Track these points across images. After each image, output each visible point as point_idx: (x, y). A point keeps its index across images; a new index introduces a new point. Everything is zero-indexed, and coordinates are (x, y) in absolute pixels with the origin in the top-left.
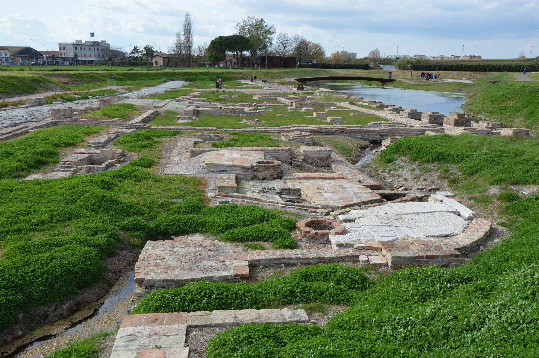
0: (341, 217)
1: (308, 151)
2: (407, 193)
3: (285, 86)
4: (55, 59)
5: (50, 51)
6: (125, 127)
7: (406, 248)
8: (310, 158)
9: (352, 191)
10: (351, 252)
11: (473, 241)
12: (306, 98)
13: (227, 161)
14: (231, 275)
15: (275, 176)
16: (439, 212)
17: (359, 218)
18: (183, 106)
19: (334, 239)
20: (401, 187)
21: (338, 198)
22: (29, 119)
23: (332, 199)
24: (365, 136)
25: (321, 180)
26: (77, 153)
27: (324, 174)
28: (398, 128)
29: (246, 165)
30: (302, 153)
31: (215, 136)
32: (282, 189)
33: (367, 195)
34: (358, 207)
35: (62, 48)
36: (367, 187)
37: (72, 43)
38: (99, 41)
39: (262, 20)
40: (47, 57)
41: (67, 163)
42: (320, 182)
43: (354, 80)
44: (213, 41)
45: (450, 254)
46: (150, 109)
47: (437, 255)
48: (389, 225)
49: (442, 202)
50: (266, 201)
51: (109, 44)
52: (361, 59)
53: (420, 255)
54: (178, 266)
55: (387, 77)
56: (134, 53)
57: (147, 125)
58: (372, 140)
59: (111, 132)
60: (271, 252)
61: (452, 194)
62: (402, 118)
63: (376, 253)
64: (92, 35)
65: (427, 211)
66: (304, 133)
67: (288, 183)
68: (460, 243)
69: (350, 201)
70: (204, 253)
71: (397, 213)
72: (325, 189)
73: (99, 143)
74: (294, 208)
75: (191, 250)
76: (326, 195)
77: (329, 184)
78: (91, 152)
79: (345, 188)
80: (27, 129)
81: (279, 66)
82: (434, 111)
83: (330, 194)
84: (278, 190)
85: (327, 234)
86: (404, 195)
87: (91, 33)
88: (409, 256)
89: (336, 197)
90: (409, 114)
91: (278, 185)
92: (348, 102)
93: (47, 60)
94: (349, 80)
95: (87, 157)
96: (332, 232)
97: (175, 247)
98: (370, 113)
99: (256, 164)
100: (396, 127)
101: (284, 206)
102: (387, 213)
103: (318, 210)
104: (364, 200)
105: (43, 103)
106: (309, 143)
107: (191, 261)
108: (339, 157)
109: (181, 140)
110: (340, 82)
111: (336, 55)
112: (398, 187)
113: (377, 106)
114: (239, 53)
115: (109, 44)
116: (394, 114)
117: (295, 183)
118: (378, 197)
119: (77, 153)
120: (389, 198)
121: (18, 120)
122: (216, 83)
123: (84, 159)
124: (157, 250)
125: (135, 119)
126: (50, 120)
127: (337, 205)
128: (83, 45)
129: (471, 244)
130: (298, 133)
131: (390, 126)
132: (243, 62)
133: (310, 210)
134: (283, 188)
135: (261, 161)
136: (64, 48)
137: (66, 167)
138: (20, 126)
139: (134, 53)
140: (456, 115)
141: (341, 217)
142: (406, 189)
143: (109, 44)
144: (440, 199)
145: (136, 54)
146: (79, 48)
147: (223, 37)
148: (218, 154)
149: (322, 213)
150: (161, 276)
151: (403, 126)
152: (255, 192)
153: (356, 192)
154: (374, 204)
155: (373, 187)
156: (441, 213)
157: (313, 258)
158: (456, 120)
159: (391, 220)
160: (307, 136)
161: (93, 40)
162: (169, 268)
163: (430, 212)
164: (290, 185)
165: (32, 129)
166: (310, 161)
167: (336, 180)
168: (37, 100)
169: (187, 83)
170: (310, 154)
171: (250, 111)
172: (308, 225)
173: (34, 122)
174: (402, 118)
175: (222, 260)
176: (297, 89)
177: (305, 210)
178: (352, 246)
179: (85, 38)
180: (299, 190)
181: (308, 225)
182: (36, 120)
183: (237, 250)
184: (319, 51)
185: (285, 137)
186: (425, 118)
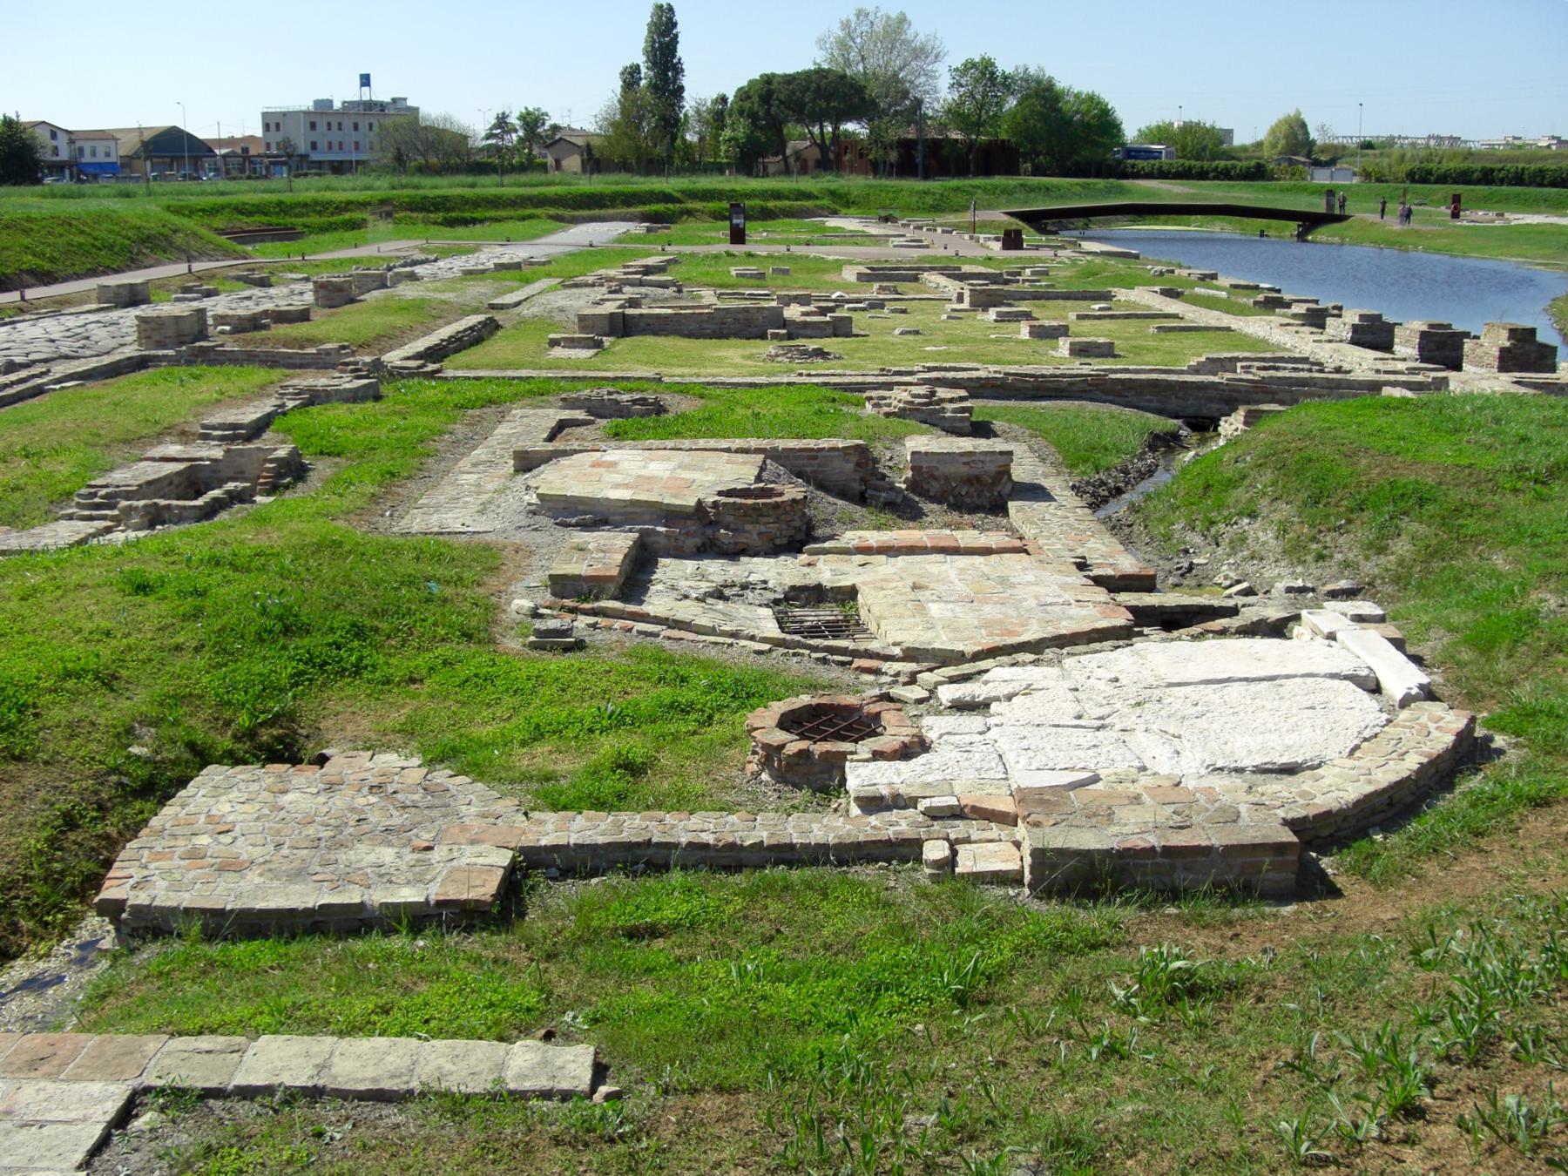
0: (947, 693)
1: (926, 454)
2: (1244, 606)
3: (967, 237)
4: (251, 162)
5: (238, 135)
6: (353, 371)
7: (1103, 815)
8: (936, 479)
9: (1036, 597)
10: (899, 825)
11: (1369, 789)
12: (1019, 274)
13: (616, 486)
14: (427, 902)
15: (778, 542)
16: (1303, 676)
17: (1009, 698)
18: (582, 302)
19: (862, 775)
20: (1238, 582)
21: (976, 623)
22: (64, 350)
23: (951, 626)
24: (1174, 403)
25: (940, 557)
26: (153, 459)
27: (958, 534)
28: (1294, 375)
29: (677, 502)
30: (909, 458)
31: (634, 402)
32: (793, 588)
33: (1084, 612)
34: (1030, 657)
35: (273, 127)
36: (1098, 581)
37: (304, 108)
38: (388, 99)
39: (902, 20)
40: (224, 156)
41: (103, 492)
42: (933, 565)
43: (1209, 217)
44: (740, 89)
45: (1257, 841)
46: (476, 311)
47: (1204, 843)
48: (1099, 723)
49: (1334, 639)
50: (712, 631)
51: (417, 109)
52: (1244, 149)
53: (1142, 844)
54: (261, 860)
55: (1319, 206)
56: (496, 136)
57: (431, 367)
58: (1196, 417)
59: (291, 390)
60: (611, 818)
61: (1379, 611)
62: (1320, 341)
63: (995, 830)
64: (365, 80)
65: (1262, 674)
66: (942, 393)
67: (820, 565)
68: (1319, 800)
69: (1010, 633)
70: (374, 817)
71: (1151, 681)
72: (941, 588)
73: (234, 426)
74: (803, 655)
75: (339, 802)
76: (935, 609)
77: (963, 571)
78: (198, 455)
79: (1012, 586)
80: (40, 381)
81: (962, 171)
82: (1436, 321)
83: (950, 606)
84: (779, 589)
85: (842, 756)
86: (1233, 612)
87: (362, 76)
88: (1099, 846)
89: (966, 616)
90: (1355, 328)
91: (782, 572)
92: (1157, 289)
93: (226, 164)
94: (1193, 217)
95: (179, 473)
96: (864, 748)
97: (285, 792)
98: (1218, 324)
99: (717, 498)
100: (1286, 374)
101: (766, 647)
102: (1117, 680)
103: (885, 666)
104: (1065, 628)
105: (140, 298)
106: (958, 425)
107: (316, 844)
108: (1046, 476)
109: (515, 416)
110: (1166, 223)
111: (1162, 133)
112: (1228, 583)
113: (1256, 303)
114: (829, 129)
115: (417, 109)
116: (1295, 329)
117: (846, 567)
118: (1122, 619)
119: (153, 459)
120: (1172, 621)
121: (27, 354)
122: (728, 223)
123: (169, 480)
124: (223, 798)
125: (406, 347)
126: (131, 351)
127: (959, 647)
128: (337, 113)
129: (1357, 803)
130: (922, 390)
131: (1265, 369)
132: (832, 157)
133: (858, 662)
134: (798, 582)
135: (739, 486)
136: (278, 126)
137: (98, 507)
138: (23, 374)
139: (496, 136)
140: (1505, 334)
141: (947, 693)
142: (1249, 592)
143: (417, 109)
144: (1326, 631)
145: (503, 139)
146: (322, 126)
147: (774, 75)
148: (596, 465)
149: (897, 674)
150: (187, 895)
151: (1310, 370)
152: (686, 597)
153: (1049, 600)
154: (1097, 646)
155: (1115, 584)
156: (1311, 680)
157: (752, 845)
158: (1503, 350)
159: (1118, 706)
160: (951, 400)
161: (366, 98)
162: (231, 866)
163: (1272, 678)
164: (827, 571)
165: (59, 381)
166: (935, 487)
167: (994, 557)
168: (121, 291)
169: (637, 228)
170: (934, 464)
171: (803, 318)
172: (789, 722)
173: (78, 358)
174: (1320, 341)
175: (426, 844)
176: (1000, 244)
177: (842, 664)
178: (911, 802)
179: (343, 92)
180: (851, 593)
181: (789, 722)
182: (88, 352)
183: (499, 807)
184: (1102, 123)
185: (876, 405)
186: (1406, 343)
